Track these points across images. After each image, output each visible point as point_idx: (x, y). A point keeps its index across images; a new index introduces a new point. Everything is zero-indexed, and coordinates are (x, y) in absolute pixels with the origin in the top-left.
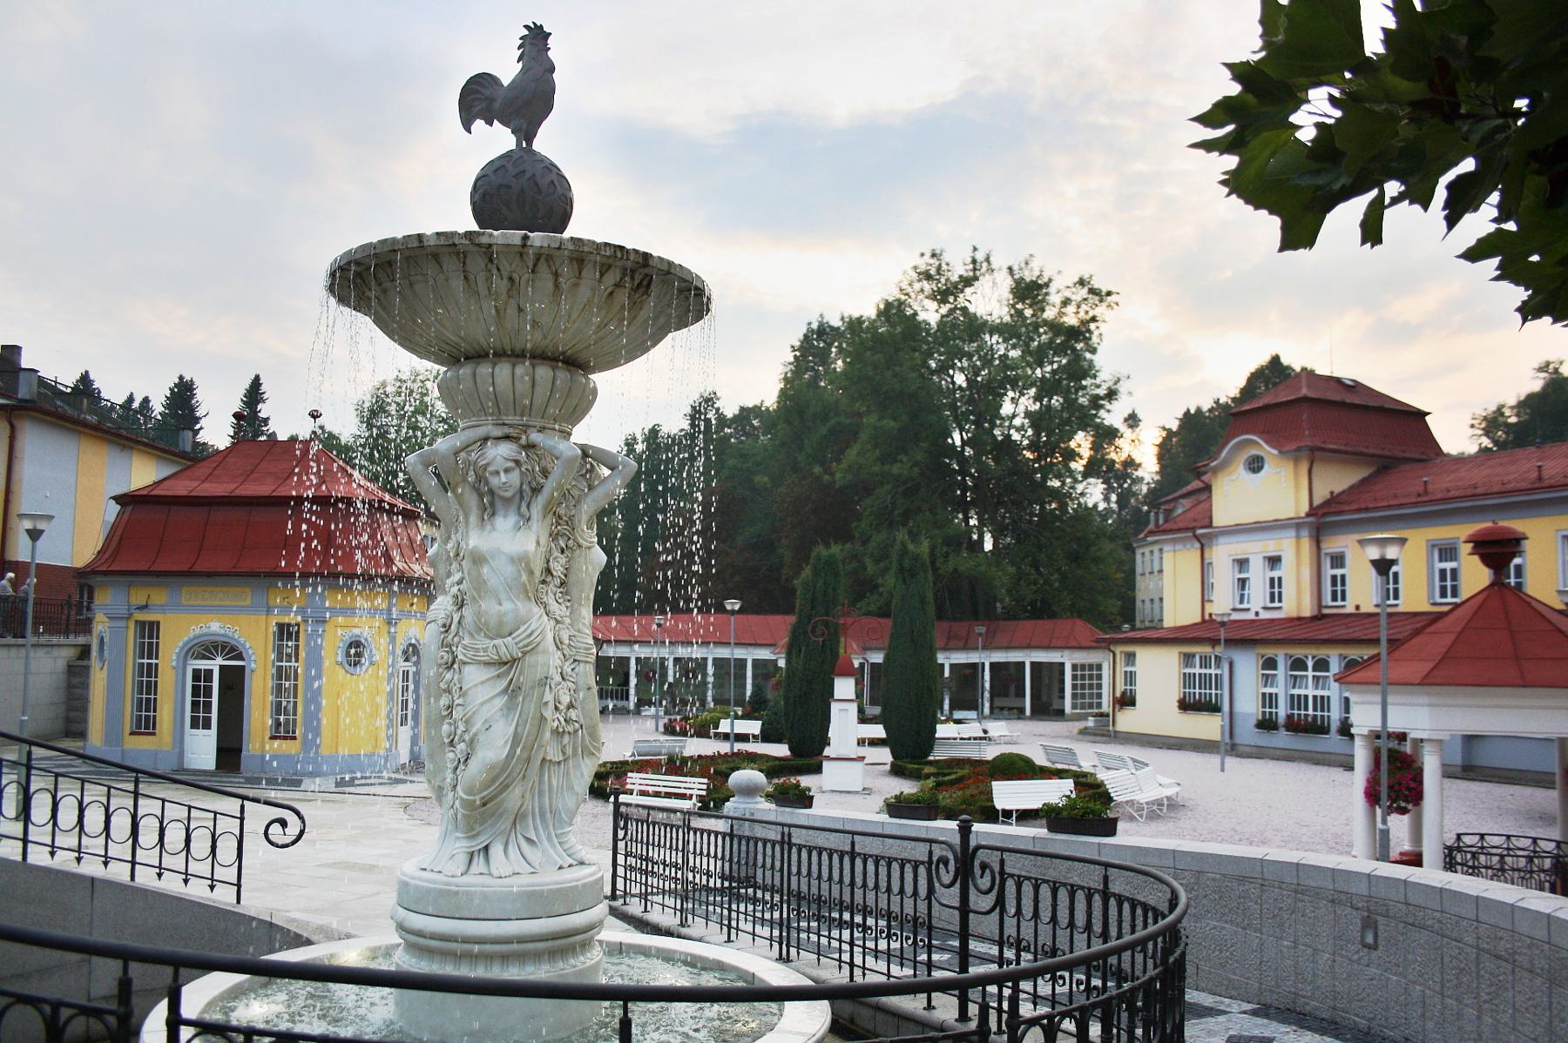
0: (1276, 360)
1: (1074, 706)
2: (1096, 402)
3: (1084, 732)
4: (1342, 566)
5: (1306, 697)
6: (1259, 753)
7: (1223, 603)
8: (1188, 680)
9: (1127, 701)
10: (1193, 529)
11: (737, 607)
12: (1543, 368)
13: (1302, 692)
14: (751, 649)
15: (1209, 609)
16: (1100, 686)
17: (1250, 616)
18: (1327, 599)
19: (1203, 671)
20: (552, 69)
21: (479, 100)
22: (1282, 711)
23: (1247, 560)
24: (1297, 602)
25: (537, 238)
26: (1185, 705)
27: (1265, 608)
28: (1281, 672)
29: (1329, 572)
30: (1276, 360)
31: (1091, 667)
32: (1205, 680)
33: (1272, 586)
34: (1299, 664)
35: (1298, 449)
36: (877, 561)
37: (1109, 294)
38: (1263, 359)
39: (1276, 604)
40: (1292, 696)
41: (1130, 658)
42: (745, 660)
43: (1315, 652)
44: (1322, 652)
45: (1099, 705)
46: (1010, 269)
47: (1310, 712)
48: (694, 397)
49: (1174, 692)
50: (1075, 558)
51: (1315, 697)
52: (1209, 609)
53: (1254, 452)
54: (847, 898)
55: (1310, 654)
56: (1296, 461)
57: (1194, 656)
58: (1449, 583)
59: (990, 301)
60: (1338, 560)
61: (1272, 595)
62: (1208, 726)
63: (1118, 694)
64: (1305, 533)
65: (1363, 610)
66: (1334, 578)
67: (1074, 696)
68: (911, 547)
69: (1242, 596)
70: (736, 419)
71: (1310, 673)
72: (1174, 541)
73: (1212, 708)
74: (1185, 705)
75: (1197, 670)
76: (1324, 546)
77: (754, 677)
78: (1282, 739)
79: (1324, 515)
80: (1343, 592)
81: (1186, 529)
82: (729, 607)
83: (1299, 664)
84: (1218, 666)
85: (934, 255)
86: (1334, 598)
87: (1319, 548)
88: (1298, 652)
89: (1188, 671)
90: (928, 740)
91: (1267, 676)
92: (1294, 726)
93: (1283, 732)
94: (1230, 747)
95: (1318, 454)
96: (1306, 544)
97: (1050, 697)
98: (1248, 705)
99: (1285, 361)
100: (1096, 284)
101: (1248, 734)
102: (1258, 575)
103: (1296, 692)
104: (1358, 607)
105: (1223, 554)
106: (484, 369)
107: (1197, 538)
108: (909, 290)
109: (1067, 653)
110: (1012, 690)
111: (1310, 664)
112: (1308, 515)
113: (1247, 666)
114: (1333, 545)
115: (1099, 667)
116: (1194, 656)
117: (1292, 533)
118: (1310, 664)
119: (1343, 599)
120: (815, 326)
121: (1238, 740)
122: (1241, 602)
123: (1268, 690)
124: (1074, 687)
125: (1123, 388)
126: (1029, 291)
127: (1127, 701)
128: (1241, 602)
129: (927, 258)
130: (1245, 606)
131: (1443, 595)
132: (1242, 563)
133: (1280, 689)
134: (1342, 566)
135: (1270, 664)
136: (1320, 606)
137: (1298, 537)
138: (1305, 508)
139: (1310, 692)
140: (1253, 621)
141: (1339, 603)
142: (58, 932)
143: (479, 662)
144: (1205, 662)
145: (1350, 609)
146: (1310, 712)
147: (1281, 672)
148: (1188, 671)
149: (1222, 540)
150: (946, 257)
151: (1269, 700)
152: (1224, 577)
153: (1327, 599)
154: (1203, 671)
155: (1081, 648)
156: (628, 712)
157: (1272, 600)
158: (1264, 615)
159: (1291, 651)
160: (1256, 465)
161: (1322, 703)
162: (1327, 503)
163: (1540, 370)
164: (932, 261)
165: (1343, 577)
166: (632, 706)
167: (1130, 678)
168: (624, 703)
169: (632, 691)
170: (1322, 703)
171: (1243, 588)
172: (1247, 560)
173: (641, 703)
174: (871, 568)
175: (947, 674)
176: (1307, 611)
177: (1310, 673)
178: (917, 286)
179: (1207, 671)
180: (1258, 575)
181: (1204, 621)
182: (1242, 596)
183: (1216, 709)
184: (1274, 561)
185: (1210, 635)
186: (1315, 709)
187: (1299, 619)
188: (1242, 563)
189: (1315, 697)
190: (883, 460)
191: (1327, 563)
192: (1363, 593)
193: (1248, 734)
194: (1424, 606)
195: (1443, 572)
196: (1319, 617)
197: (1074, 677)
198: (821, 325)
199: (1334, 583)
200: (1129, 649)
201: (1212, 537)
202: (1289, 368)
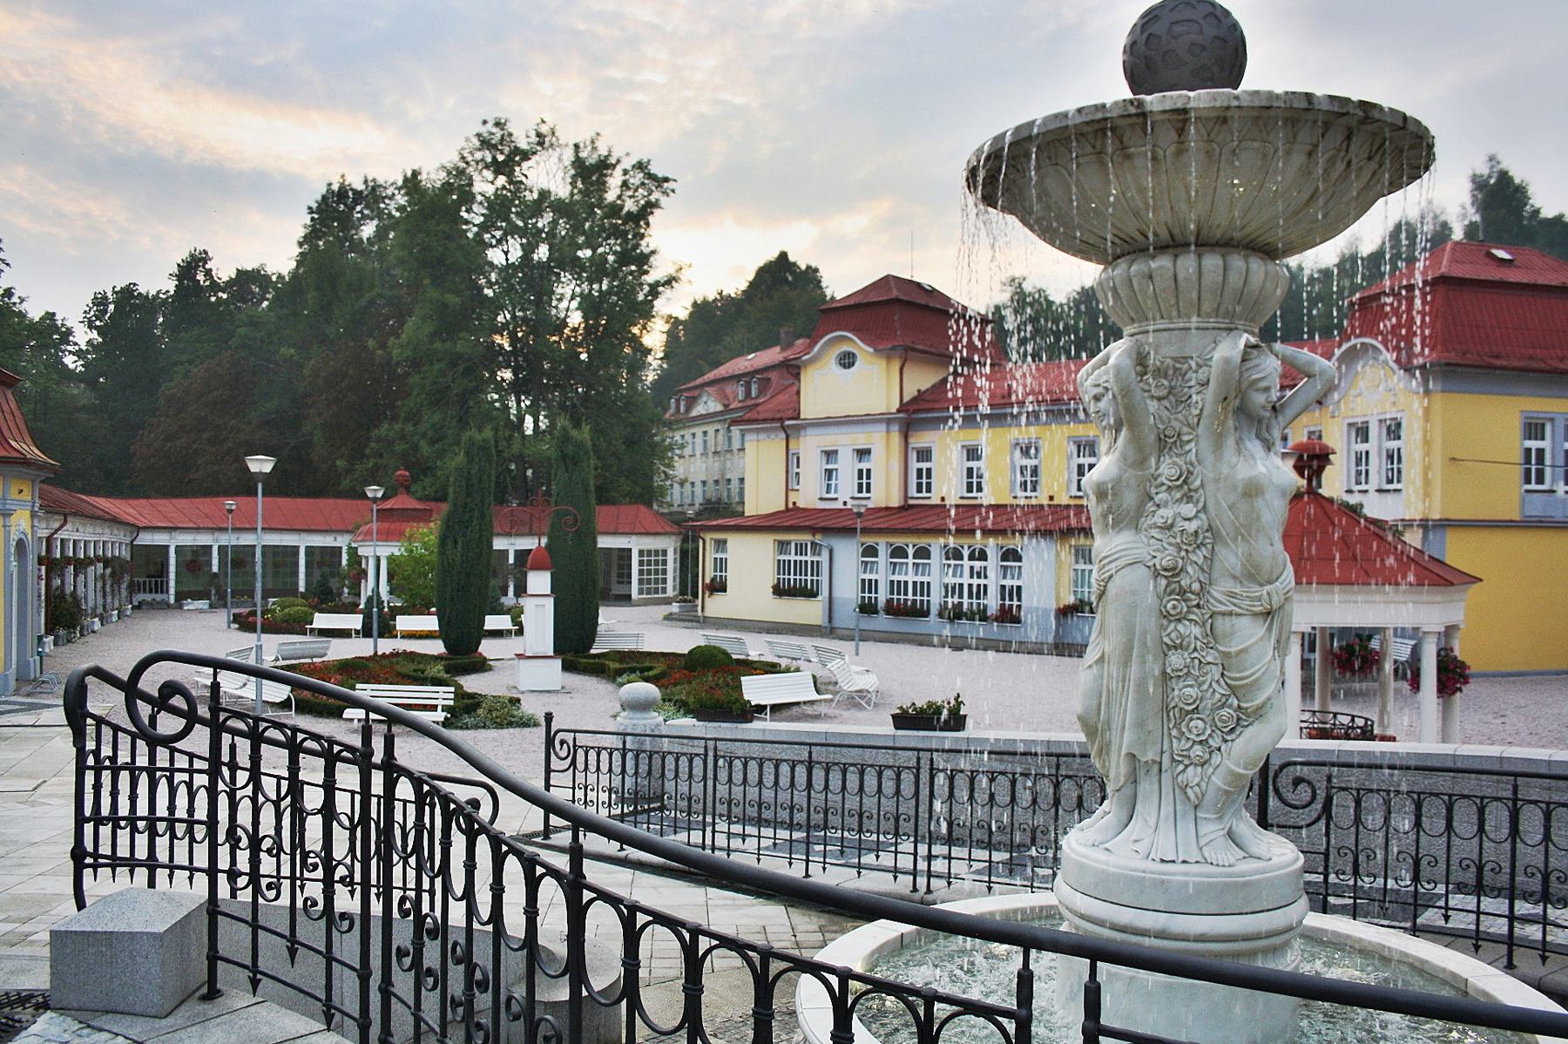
0: (783, 256)
1: (641, 592)
2: (654, 291)
3: (669, 617)
4: (929, 459)
5: (961, 585)
6: (865, 636)
7: (809, 495)
8: (782, 566)
9: (718, 587)
10: (781, 420)
11: (380, 495)
13: (902, 578)
14: (304, 535)
15: (793, 497)
16: (665, 572)
17: (839, 505)
18: (913, 492)
19: (799, 558)
22: (882, 596)
23: (836, 452)
24: (886, 492)
25: (1199, 98)
26: (779, 591)
28: (883, 557)
29: (914, 465)
30: (783, 256)
31: (657, 553)
32: (800, 567)
33: (860, 477)
34: (899, 552)
35: (893, 348)
36: (433, 442)
37: (666, 180)
38: (772, 255)
39: (864, 495)
40: (1003, 587)
41: (721, 545)
42: (211, 547)
43: (916, 540)
44: (923, 541)
45: (664, 590)
46: (577, 146)
47: (910, 596)
48: (181, 255)
49: (768, 577)
50: (630, 443)
51: (915, 583)
52: (793, 497)
53: (846, 348)
54: (1497, 853)
55: (910, 543)
56: (889, 359)
57: (789, 543)
59: (548, 176)
60: (925, 454)
61: (860, 485)
62: (809, 611)
63: (708, 581)
64: (895, 428)
66: (920, 471)
67: (641, 581)
68: (574, 433)
69: (829, 486)
70: (231, 283)
71: (911, 560)
72: (758, 431)
73: (810, 593)
74: (779, 591)
75: (792, 557)
76: (911, 440)
77: (297, 564)
78: (883, 622)
79: (915, 412)
80: (868, 485)
81: (773, 420)
82: (370, 495)
83: (899, 552)
85: (497, 124)
86: (919, 490)
87: (906, 442)
88: (899, 541)
89: (782, 557)
90: (589, 630)
91: (1005, 568)
92: (894, 610)
93: (882, 615)
94: (829, 630)
95: (911, 354)
96: (896, 438)
97: (608, 582)
98: (848, 591)
99: (792, 258)
100: (653, 169)
101: (847, 616)
102: (847, 467)
103: (896, 578)
104: (1051, 498)
105: (810, 446)
106: (1237, 261)
107: (784, 428)
108: (470, 158)
109: (634, 538)
110: (317, 558)
111: (911, 551)
112: (899, 411)
113: (847, 553)
114: (921, 440)
115: (665, 553)
116: (789, 543)
117: (883, 427)
118: (911, 551)
119: (929, 491)
120: (335, 187)
121: (836, 623)
122: (828, 491)
123: (867, 576)
124: (641, 572)
125: (684, 276)
126: (591, 172)
127: (718, 587)
128: (828, 491)
129: (490, 127)
130: (832, 495)
132: (830, 455)
133: (882, 573)
134: (929, 459)
135: (871, 551)
136: (906, 497)
137: (888, 432)
138: (897, 405)
139: (910, 578)
141: (924, 494)
143: (1255, 614)
144: (801, 549)
145: (935, 500)
146: (910, 596)
147: (883, 557)
148: (782, 557)
149: (810, 431)
150: (510, 127)
151: (869, 586)
152: (811, 468)
153: (913, 492)
154: (799, 558)
155: (648, 534)
156: (168, 606)
157: (860, 491)
159: (892, 540)
160: (847, 361)
161: (924, 588)
162: (914, 400)
164: (494, 130)
165: (929, 470)
166: (172, 600)
167: (721, 564)
168: (164, 596)
169: (172, 583)
170: (924, 588)
171: (830, 479)
172: (836, 452)
173: (181, 597)
174: (425, 449)
175: (511, 560)
176: (895, 502)
177: (911, 560)
178: (478, 155)
179: (803, 558)
180: (847, 467)
181: (787, 509)
182: (829, 486)
183: (812, 594)
184: (863, 453)
185: (787, 522)
186: (915, 594)
187: (887, 509)
188: (830, 455)
189: (915, 583)
190: (435, 335)
191: (913, 456)
193: (847, 616)
196: (906, 507)
197: (641, 563)
198: (342, 187)
199: (919, 476)
200: (720, 536)
201: (798, 428)
202: (794, 264)
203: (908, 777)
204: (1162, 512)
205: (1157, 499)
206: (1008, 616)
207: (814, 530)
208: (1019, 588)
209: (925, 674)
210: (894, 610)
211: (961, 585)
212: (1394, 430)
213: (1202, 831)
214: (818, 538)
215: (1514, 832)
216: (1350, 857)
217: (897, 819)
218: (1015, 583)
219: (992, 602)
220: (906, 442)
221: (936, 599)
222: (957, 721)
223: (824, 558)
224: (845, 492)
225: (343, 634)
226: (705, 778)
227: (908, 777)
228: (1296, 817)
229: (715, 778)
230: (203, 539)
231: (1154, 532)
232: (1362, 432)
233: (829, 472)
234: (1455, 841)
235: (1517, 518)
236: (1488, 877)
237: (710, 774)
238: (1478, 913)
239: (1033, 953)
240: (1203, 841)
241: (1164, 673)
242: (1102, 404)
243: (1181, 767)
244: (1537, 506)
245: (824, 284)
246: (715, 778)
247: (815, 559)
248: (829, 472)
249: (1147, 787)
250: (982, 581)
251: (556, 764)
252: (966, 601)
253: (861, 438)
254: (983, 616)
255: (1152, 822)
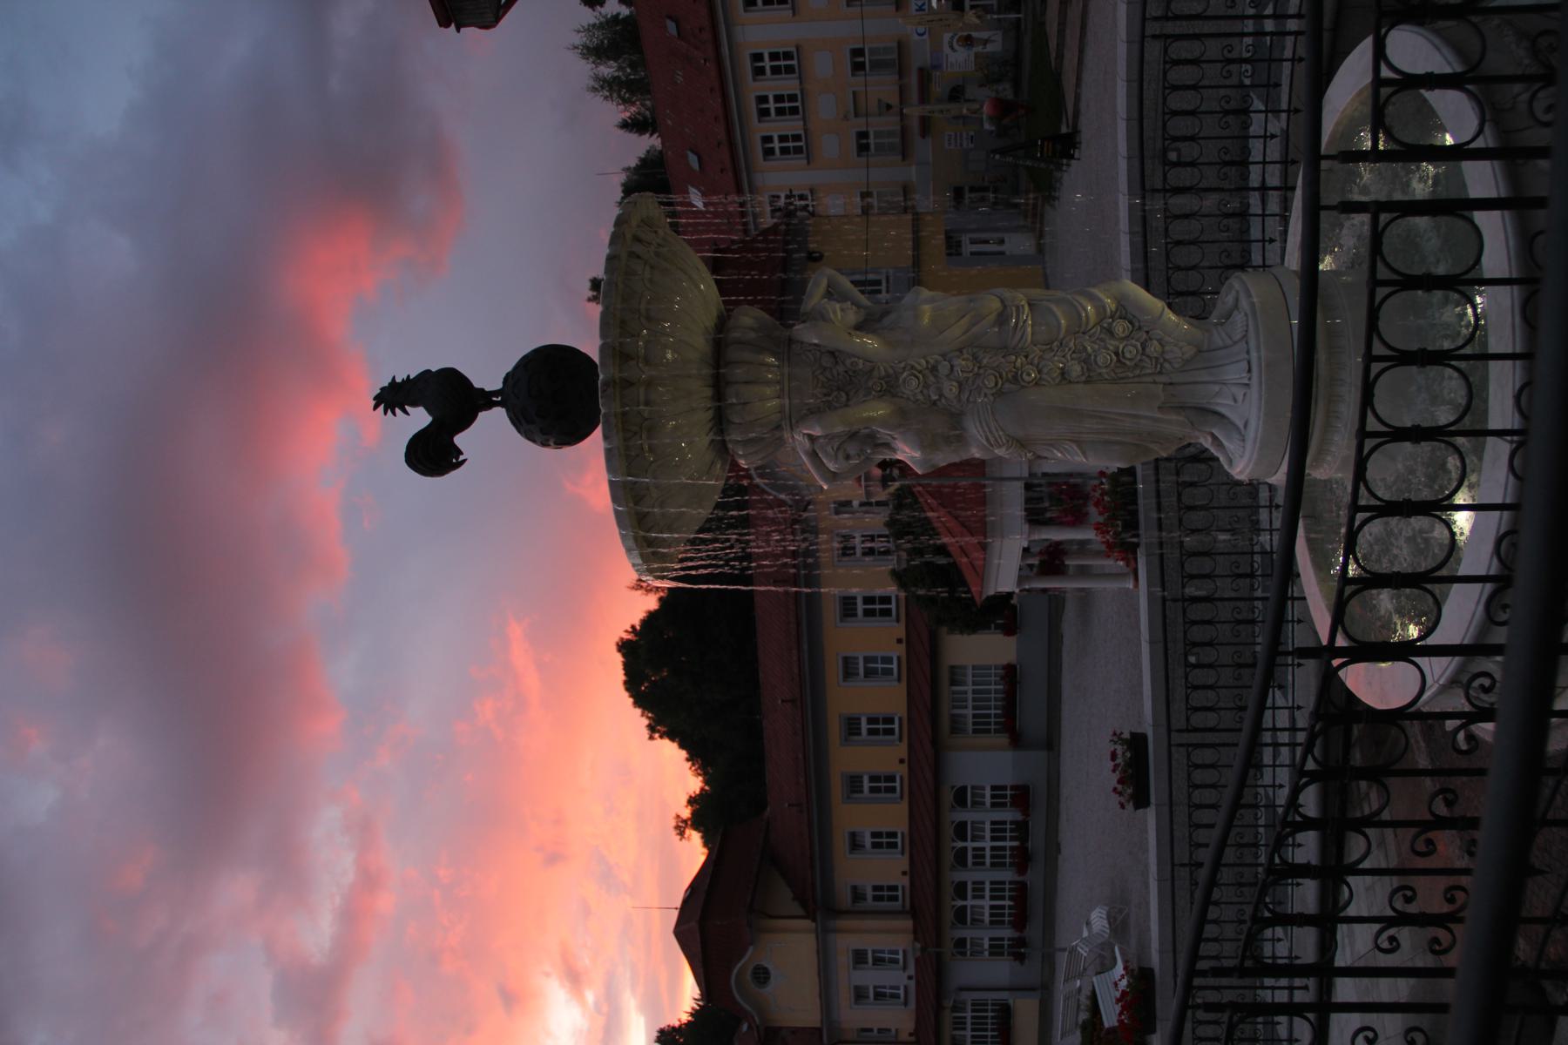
5: (992, 907)
12: (680, 831)
13: (987, 912)
17: (912, 983)
18: (897, 905)
19: (969, 1026)
20: (428, 371)
21: (432, 455)
22: (1007, 933)
23: (857, 988)
24: (894, 936)
27: (905, 968)
28: (968, 933)
29: (870, 903)
44: (948, 831)
47: (1007, 903)
53: (748, 976)
55: (953, 844)
57: (953, 1038)
58: (883, 785)
65: (906, 868)
66: (876, 898)
78: (1033, 932)
83: (960, 914)
84: (963, 1010)
86: (895, 898)
87: (847, 912)
88: (949, 916)
92: (1020, 921)
94: (1045, 990)
98: (1001, 970)
102: (870, 977)
103: (987, 918)
104: (904, 873)
111: (960, 844)
112: (814, 920)
114: (844, 898)
118: (960, 844)
130: (901, 992)
131: (893, 790)
132: (860, 995)
133: (985, 936)
138: (807, 923)
140: (918, 983)
141: (900, 893)
142: (1429, 878)
145: (906, 881)
147: (968, 933)
151: (996, 949)
153: (897, 905)
154: (969, 1026)
158: (911, 971)
160: (762, 975)
163: (682, 834)
170: (997, 887)
176: (908, 923)
179: (969, 1021)
180: (870, 977)
186: (1003, 898)
191: (861, 906)
192: (891, 869)
194: (903, 808)
195: (871, 732)
196: (914, 912)
200: (948, 797)
203: (1180, 50)
204: (946, 392)
205: (935, 397)
206: (1021, 797)
207: (939, 1009)
208: (994, 788)
209: (1088, 774)
210: (1020, 921)
211: (992, 907)
213: (1221, 344)
214: (949, 1003)
216: (1241, 627)
217: (1240, 666)
218: (988, 793)
219: (1009, 815)
220: (847, 912)
221: (1007, 875)
222: (1137, 743)
223: (969, 997)
224: (898, 978)
227: (1180, 50)
231: (964, 397)
233: (879, 996)
234: (1220, 683)
236: (1233, 105)
238: (1264, 163)
239: (1324, 202)
240: (1229, 342)
241: (1086, 382)
242: (852, 452)
243: (1167, 365)
245: (677, 1024)
247: (969, 1008)
248: (879, 996)
250: (987, 886)
252: (1008, 844)
253: (843, 960)
254: (1022, 829)
255: (1217, 388)
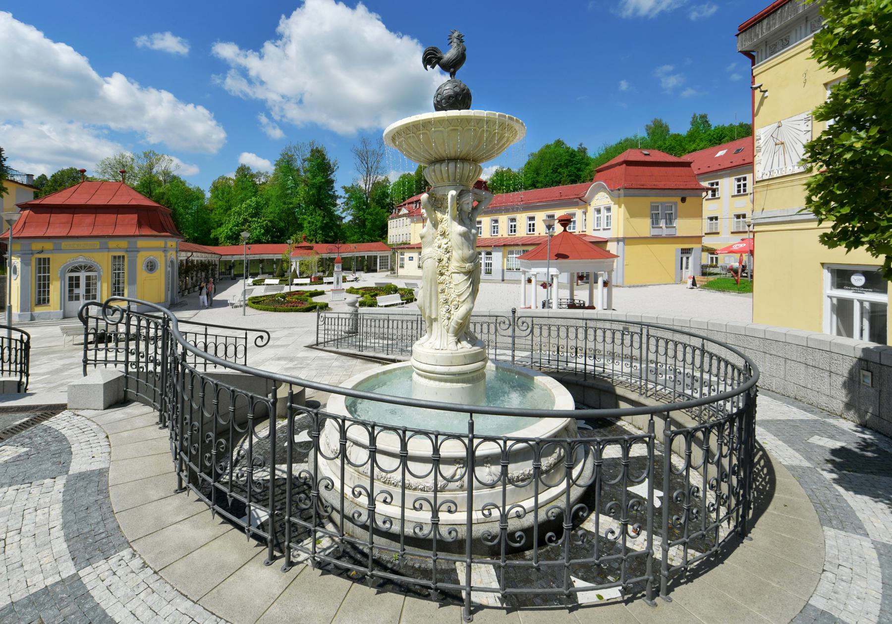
9: (402, 267)
60: (496, 221)
200: (489, 250)
212: (609, 209)
215: (586, 338)
225: (306, 284)
226: (641, 347)
228: (524, 334)
229: (648, 349)
230: (362, 254)
232: (599, 211)
235: (649, 236)
237: (644, 346)
244: (656, 232)
246: (648, 349)
249: (434, 324)
251: (320, 323)
